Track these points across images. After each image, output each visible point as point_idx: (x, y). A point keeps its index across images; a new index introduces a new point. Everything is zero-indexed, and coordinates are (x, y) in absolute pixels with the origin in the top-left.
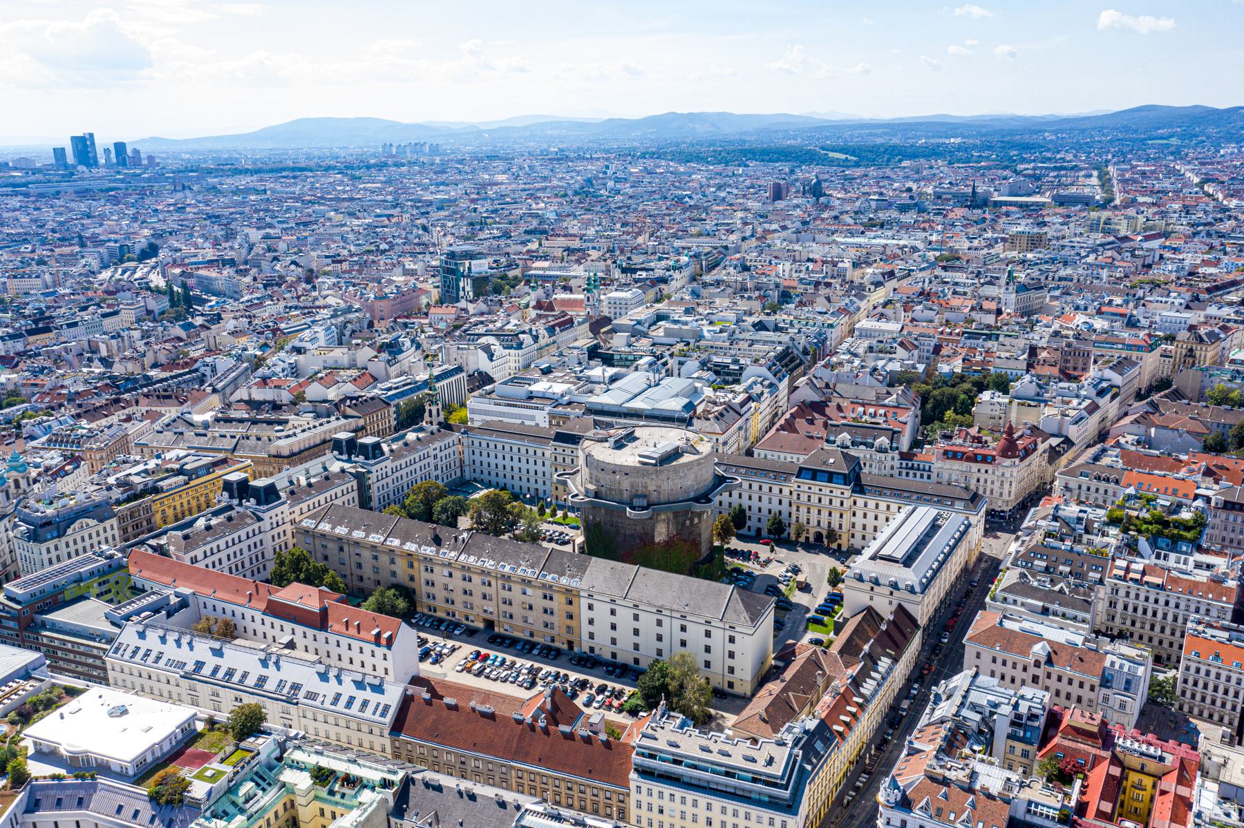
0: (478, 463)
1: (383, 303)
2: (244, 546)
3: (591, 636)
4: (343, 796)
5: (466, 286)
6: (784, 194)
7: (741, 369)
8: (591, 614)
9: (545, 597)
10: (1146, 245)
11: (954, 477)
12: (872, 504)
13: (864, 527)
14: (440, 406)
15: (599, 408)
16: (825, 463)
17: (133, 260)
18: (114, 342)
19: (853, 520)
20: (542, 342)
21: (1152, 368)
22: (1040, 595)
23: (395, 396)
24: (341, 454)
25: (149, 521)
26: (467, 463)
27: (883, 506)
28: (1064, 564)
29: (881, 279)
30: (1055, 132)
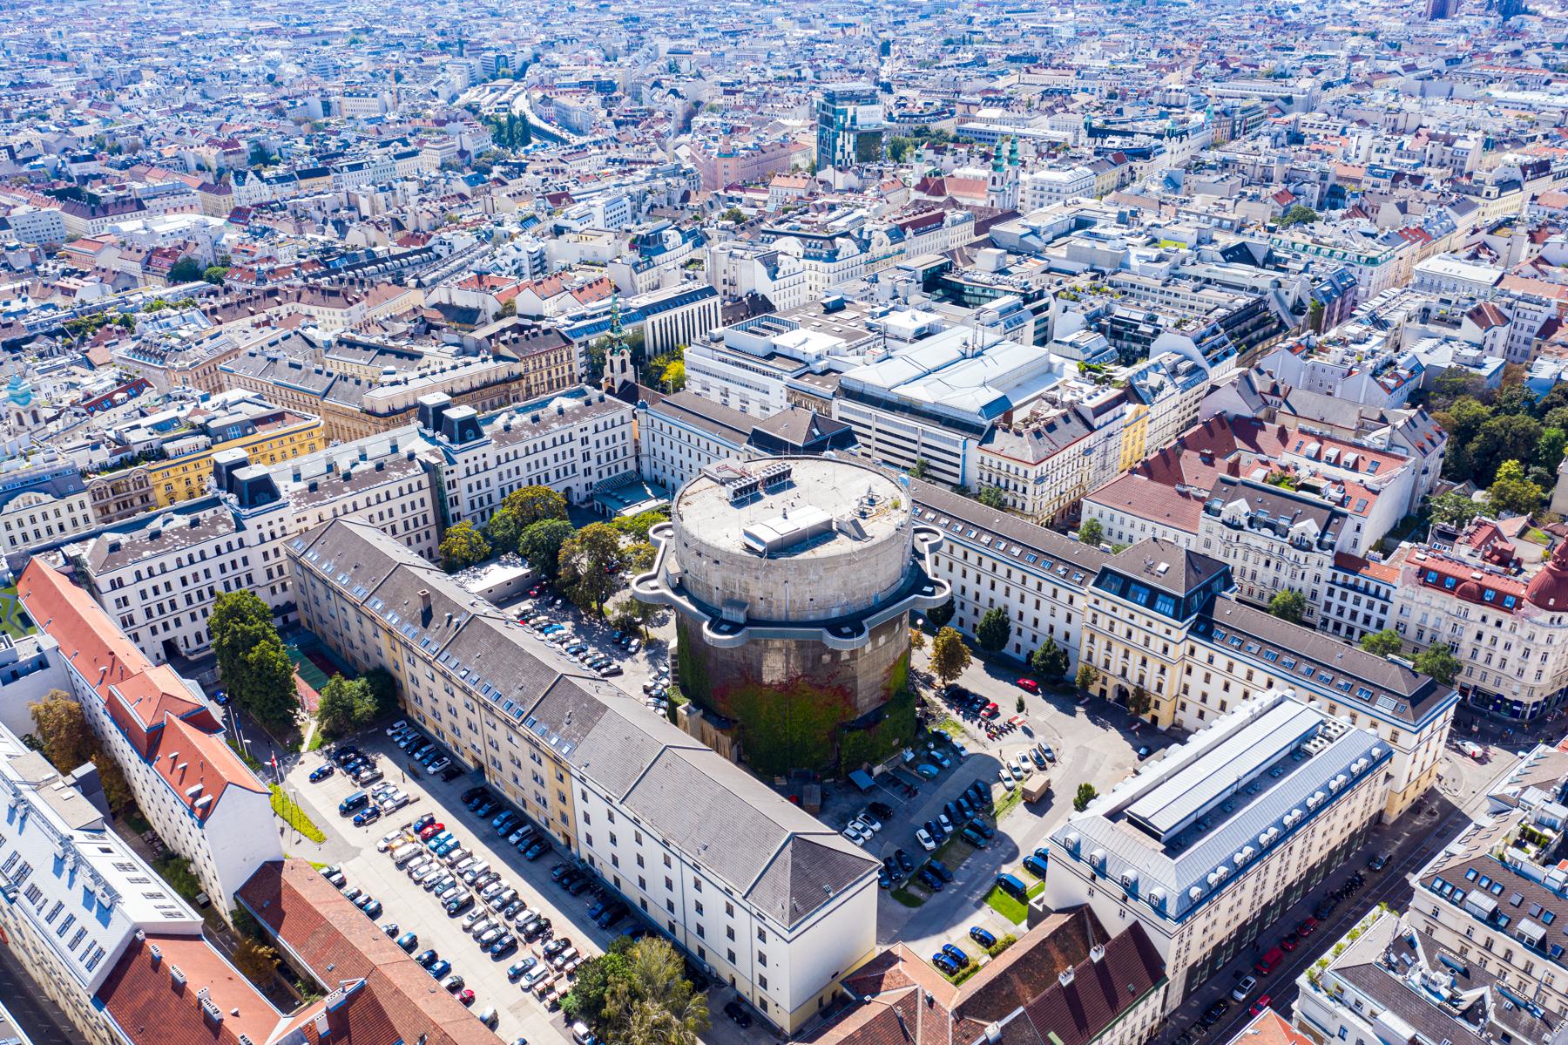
1: (730, 162)
2: (549, 454)
5: (847, 143)
6: (1451, 8)
7: (1157, 332)
11: (1430, 623)
12: (1221, 661)
13: (1204, 698)
14: (627, 357)
15: (858, 388)
16: (1149, 569)
17: (508, 76)
18: (381, 196)
19: (1186, 679)
20: (876, 251)
22: (1415, 1009)
23: (586, 330)
24: (426, 427)
25: (145, 498)
26: (644, 451)
27: (1240, 670)
28: (1534, 918)
29: (1518, 175)
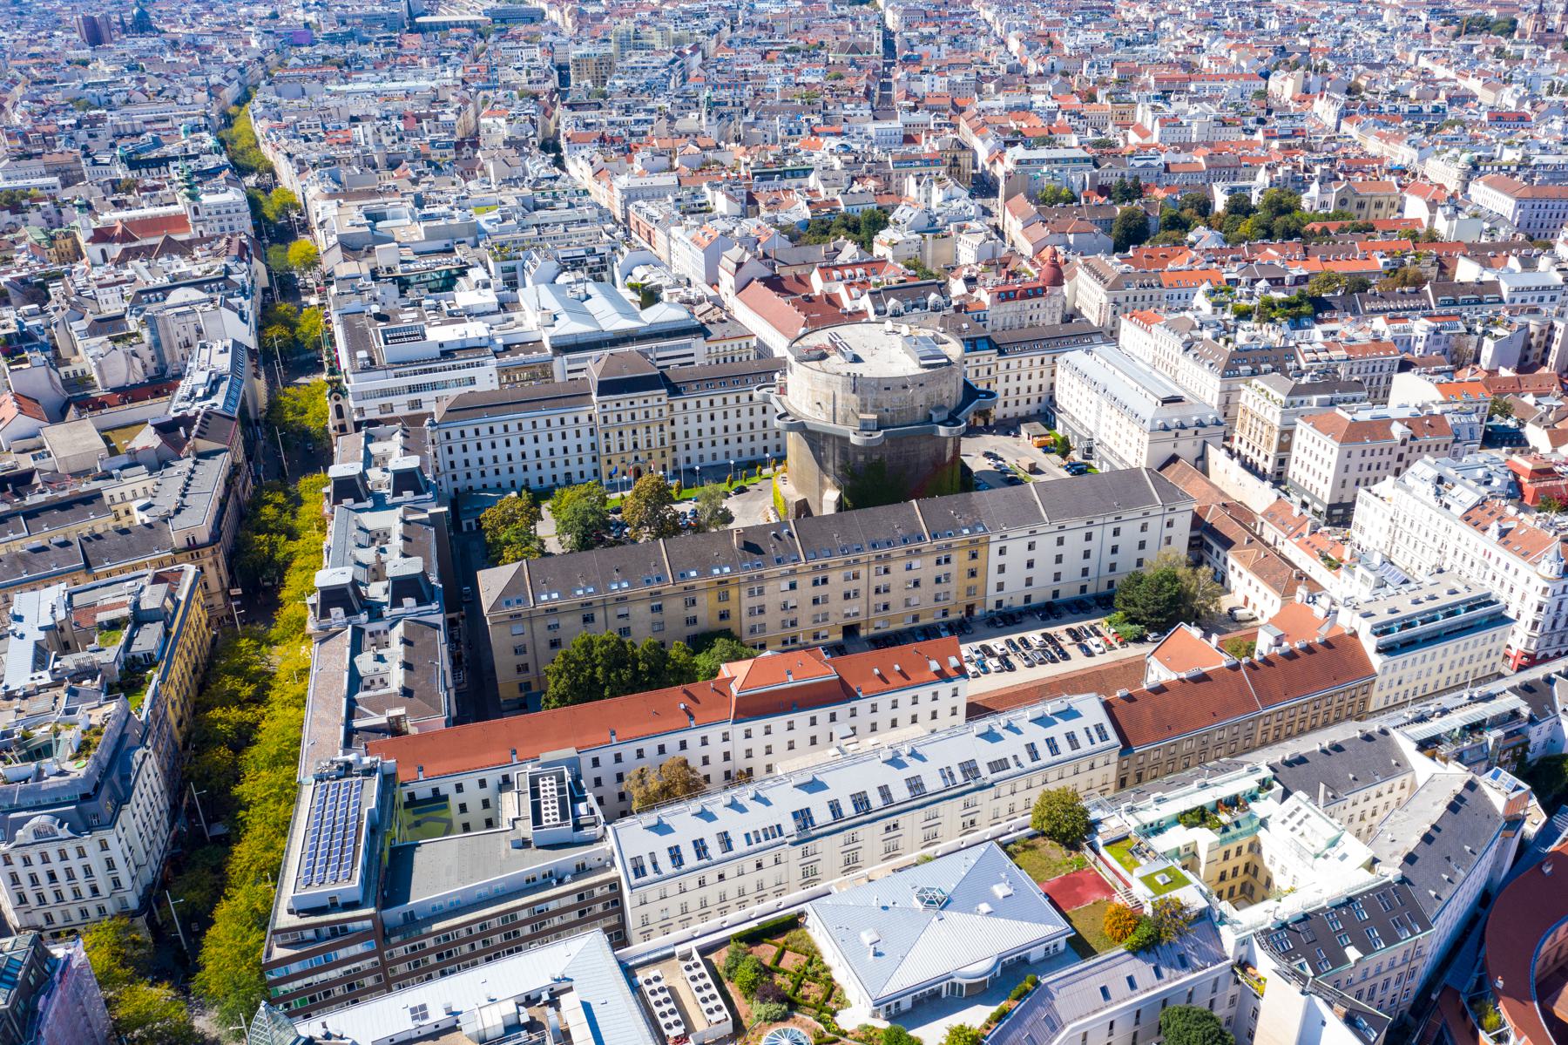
4: (1237, 825)
6: (105, 34)
8: (1002, 560)
15: (571, 341)
24: (358, 499)
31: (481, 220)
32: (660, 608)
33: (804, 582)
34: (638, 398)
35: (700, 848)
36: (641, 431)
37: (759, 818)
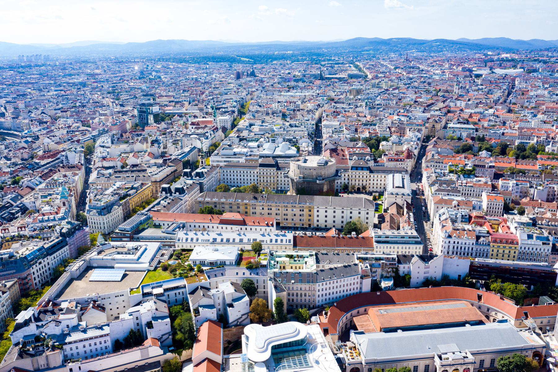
0: (226, 179)
3: (318, 221)
5: (151, 119)
6: (241, 76)
8: (318, 214)
9: (300, 210)
10: (393, 92)
12: (376, 176)
21: (80, 191)
24: (188, 177)
30: (327, 48)
31: (274, 128)
32: (231, 207)
33: (266, 208)
34: (269, 169)
35: (192, 239)
36: (269, 178)
37: (206, 237)
